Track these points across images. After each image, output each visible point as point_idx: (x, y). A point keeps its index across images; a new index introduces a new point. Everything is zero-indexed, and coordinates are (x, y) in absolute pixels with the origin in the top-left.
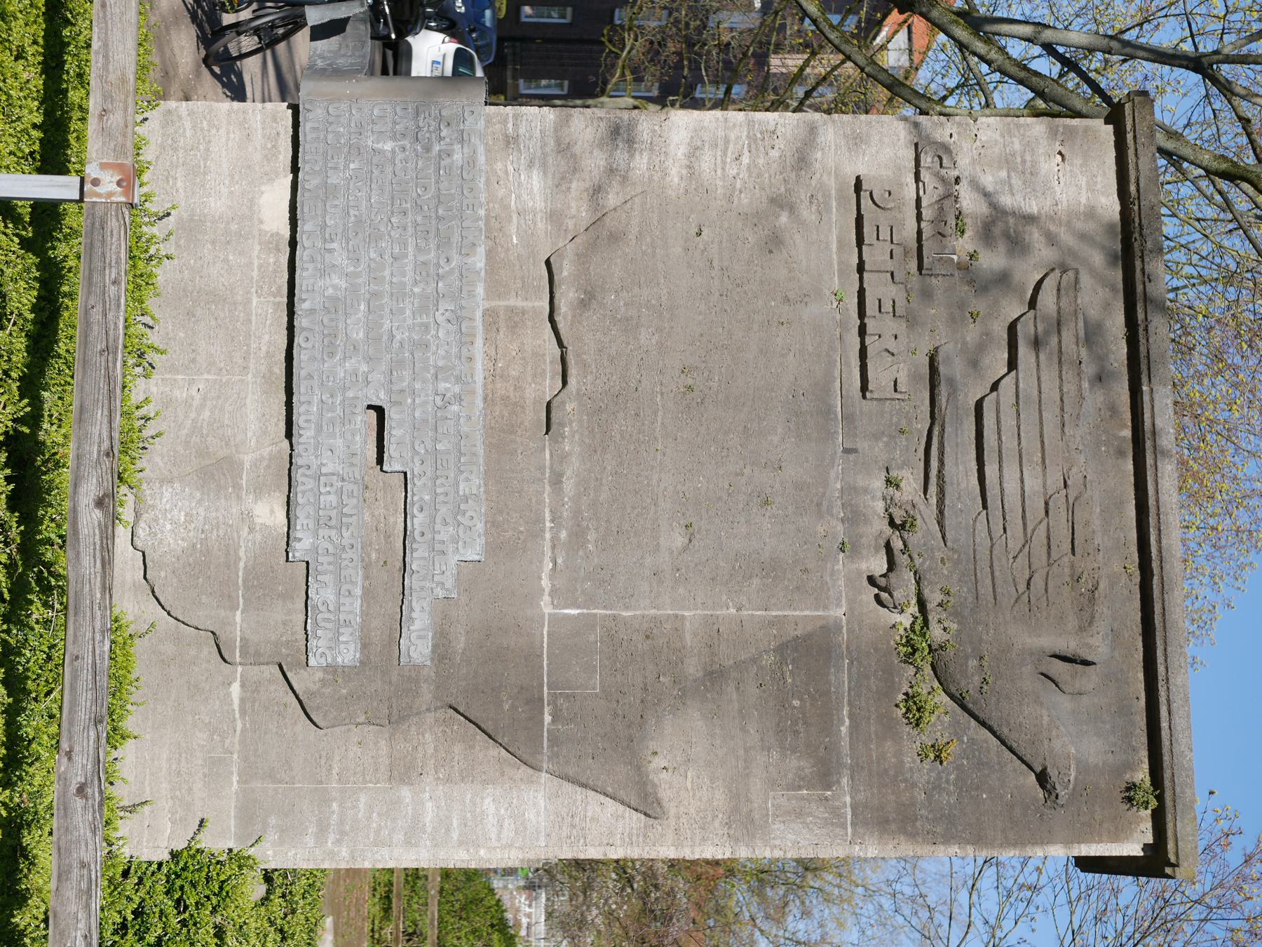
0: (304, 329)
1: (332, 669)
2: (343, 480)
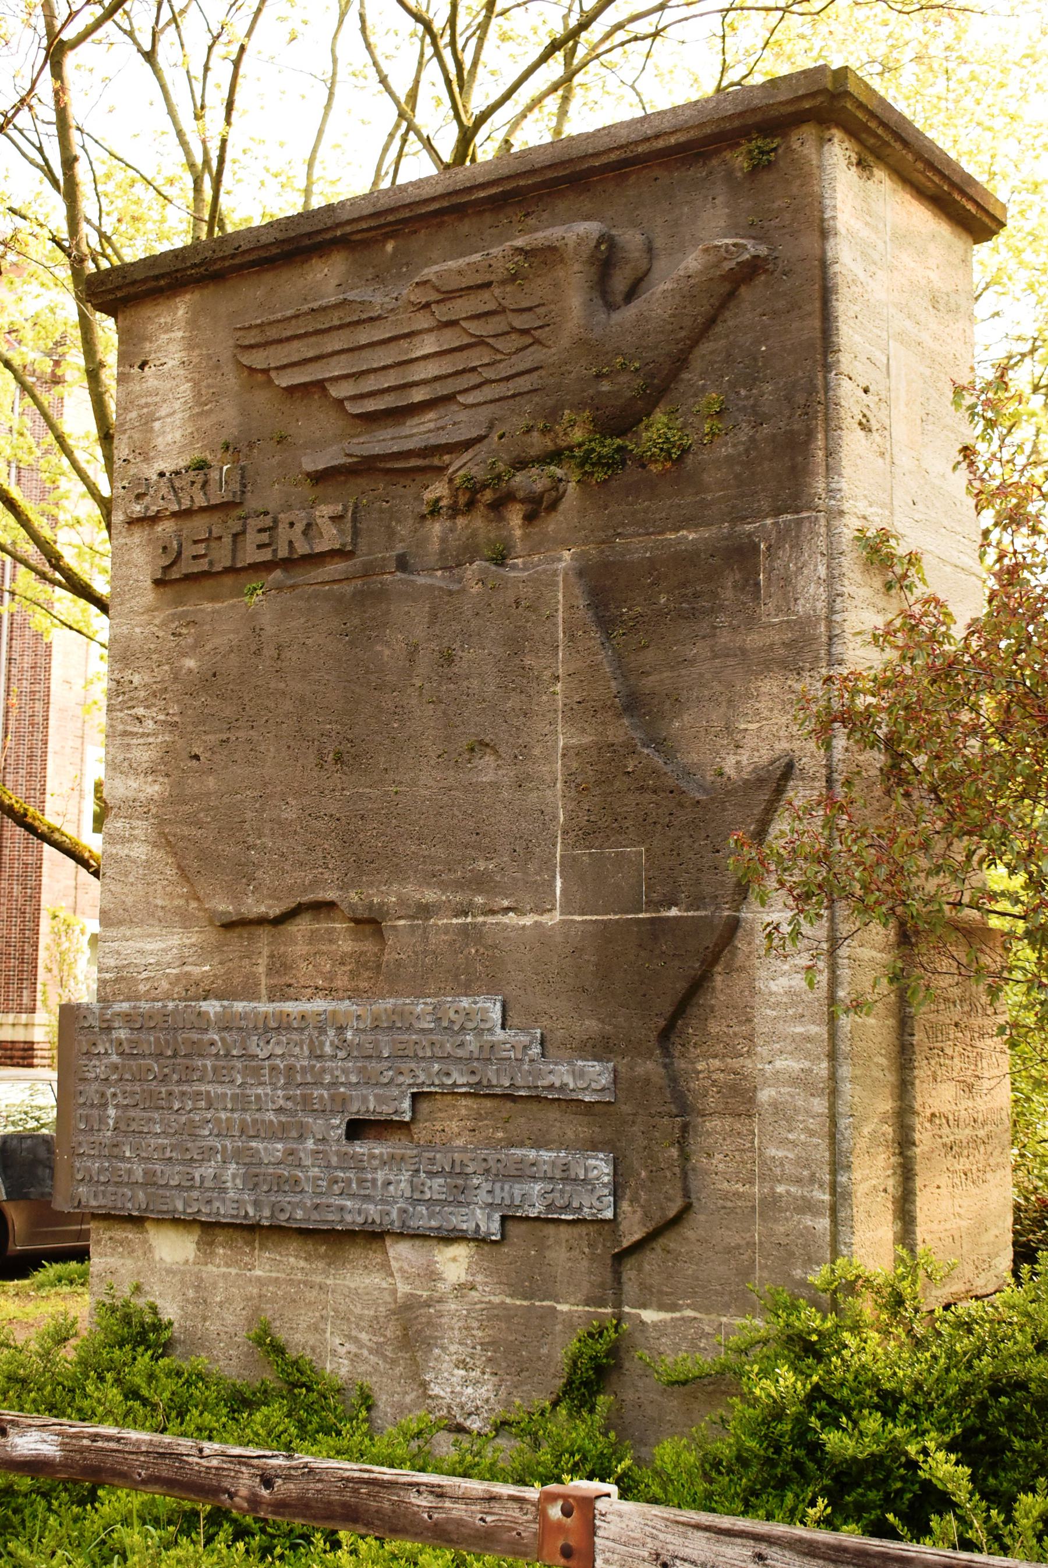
0: (272, 1216)
1: (617, 1191)
2: (417, 1171)
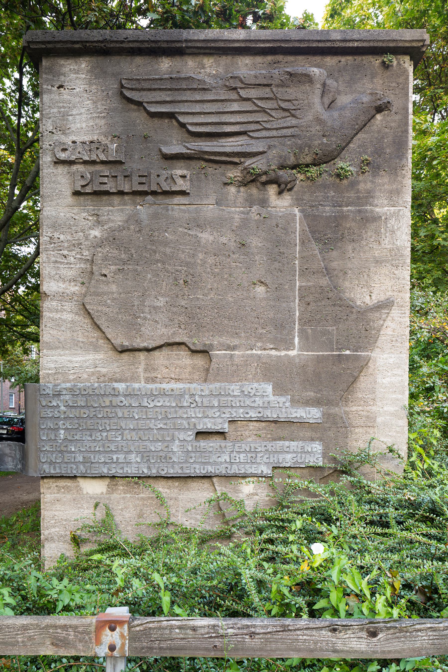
0: (158, 471)
